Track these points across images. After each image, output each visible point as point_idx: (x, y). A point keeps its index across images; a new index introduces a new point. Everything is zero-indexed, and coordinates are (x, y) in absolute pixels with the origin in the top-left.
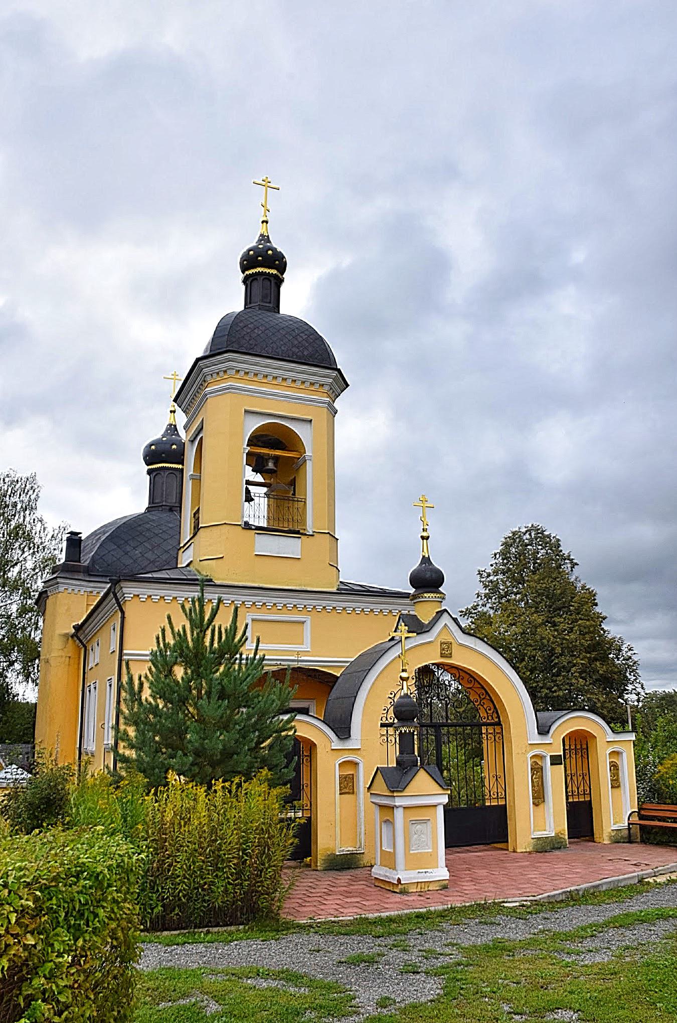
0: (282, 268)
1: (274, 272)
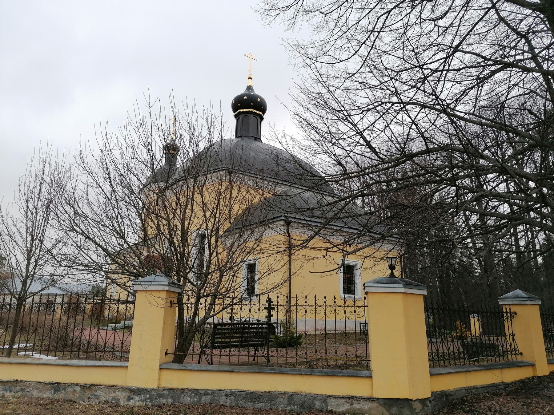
0: (264, 111)
1: (261, 113)
